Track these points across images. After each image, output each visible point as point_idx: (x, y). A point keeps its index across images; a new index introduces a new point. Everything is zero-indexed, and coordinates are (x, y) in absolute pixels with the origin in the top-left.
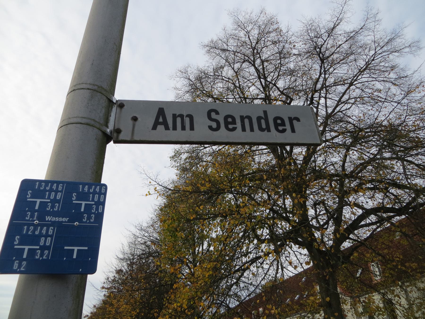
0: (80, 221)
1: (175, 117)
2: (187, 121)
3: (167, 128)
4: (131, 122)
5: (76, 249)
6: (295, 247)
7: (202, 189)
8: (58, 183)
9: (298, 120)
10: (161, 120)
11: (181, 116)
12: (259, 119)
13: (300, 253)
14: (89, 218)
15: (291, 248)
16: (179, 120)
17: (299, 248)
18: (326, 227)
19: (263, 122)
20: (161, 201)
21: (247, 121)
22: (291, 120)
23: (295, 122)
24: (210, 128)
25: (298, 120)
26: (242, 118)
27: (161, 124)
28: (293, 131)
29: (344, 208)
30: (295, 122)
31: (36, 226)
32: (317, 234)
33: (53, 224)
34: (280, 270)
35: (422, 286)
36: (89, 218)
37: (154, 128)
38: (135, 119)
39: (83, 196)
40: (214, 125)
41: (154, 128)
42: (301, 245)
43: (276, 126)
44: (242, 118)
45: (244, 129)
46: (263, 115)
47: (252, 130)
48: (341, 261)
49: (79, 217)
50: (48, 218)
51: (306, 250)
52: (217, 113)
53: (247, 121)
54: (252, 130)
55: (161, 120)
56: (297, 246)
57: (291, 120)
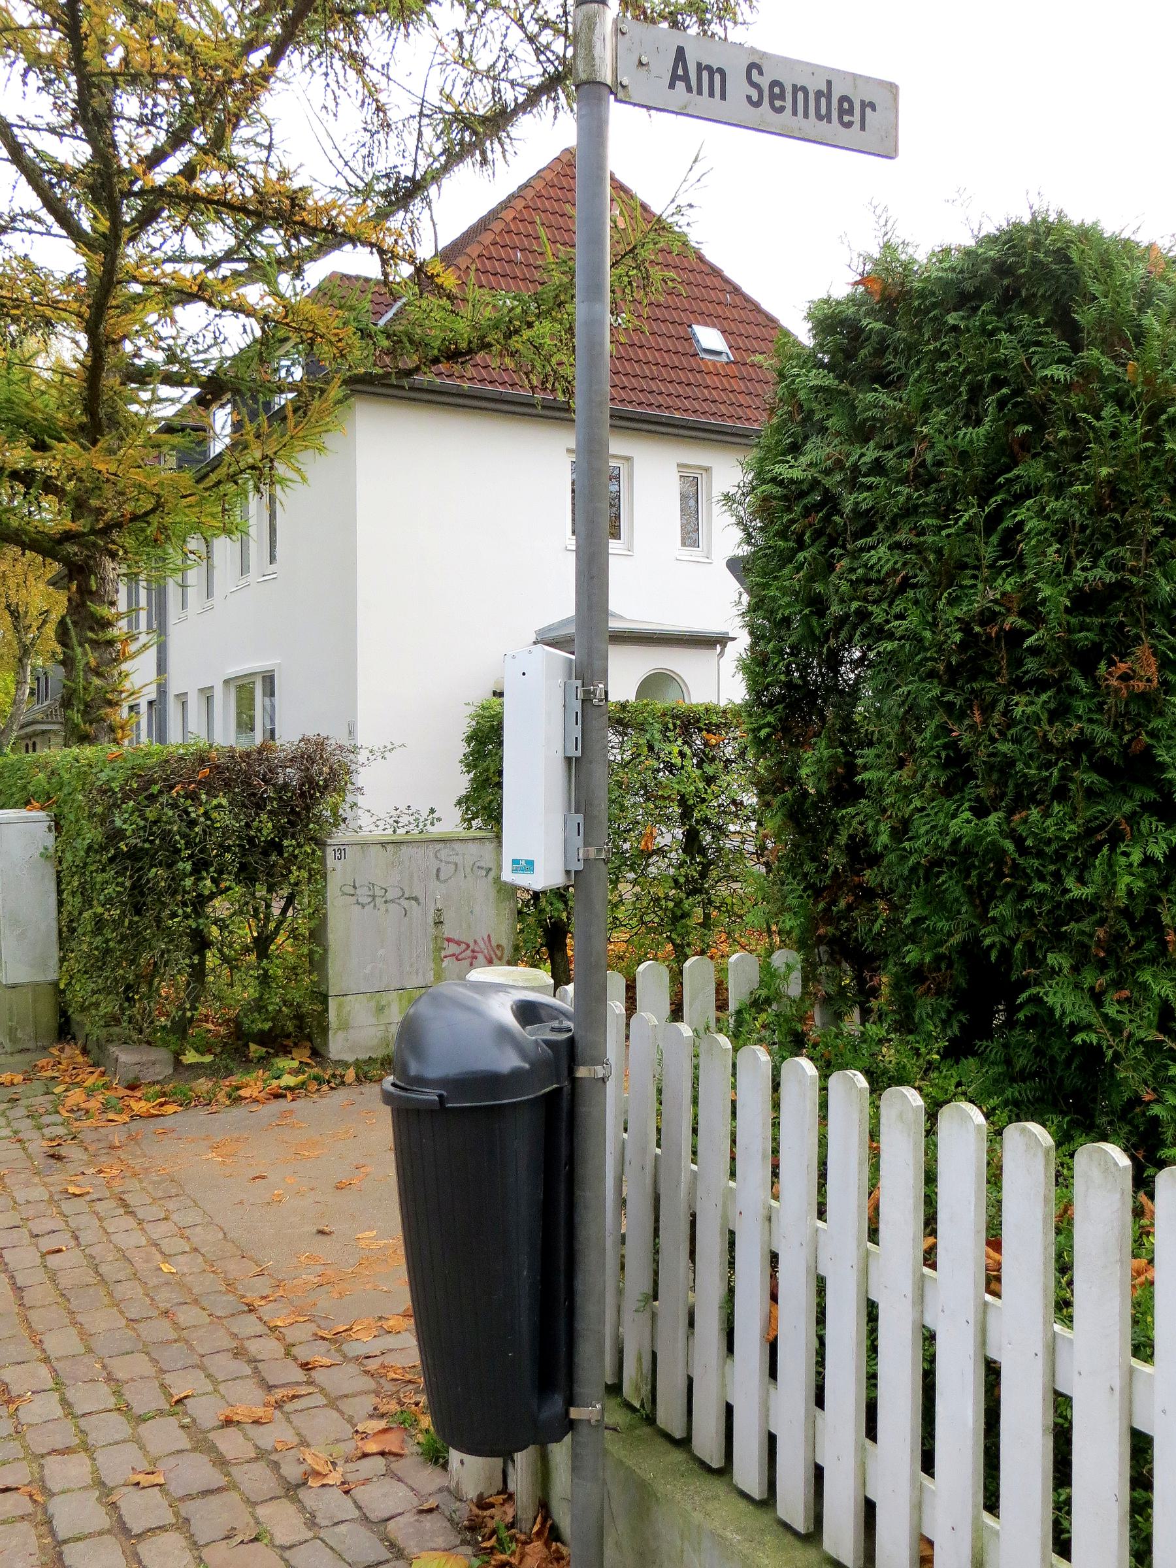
3: (689, 89)
7: (178, 224)
10: (680, 72)
12: (819, 94)
20: (1026, 220)
21: (800, 95)
22: (863, 105)
24: (749, 98)
25: (873, 107)
27: (680, 78)
28: (863, 128)
29: (862, 800)
30: (868, 110)
35: (1162, 988)
43: (842, 112)
44: (795, 89)
45: (795, 113)
46: (825, 89)
47: (806, 115)
52: (761, 73)
53: (800, 95)
54: (806, 115)
55: (680, 72)
57: (863, 105)
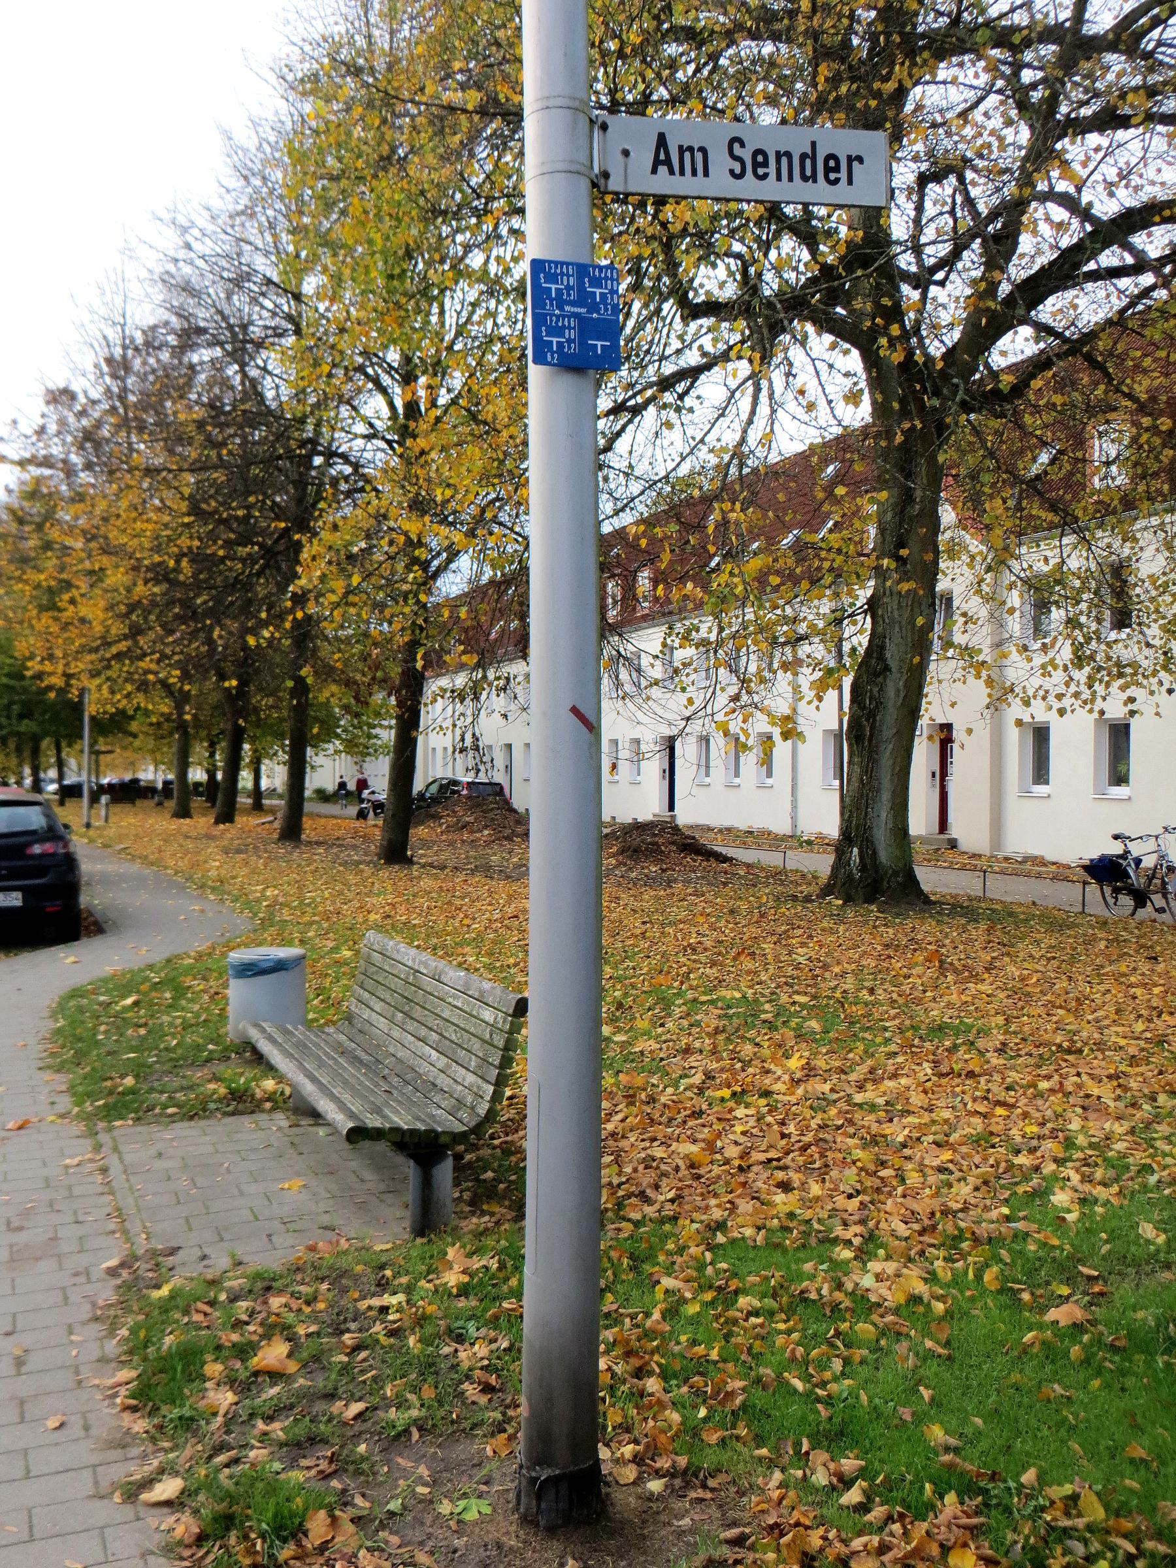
0: (598, 313)
1: (682, 150)
2: (699, 157)
3: (672, 172)
4: (621, 158)
5: (599, 343)
6: (820, 342)
8: (568, 264)
9: (860, 159)
10: (662, 157)
11: (691, 149)
13: (831, 366)
14: (606, 310)
15: (803, 343)
16: (687, 155)
17: (833, 347)
18: (940, 276)
19: (808, 162)
21: (784, 160)
22: (850, 159)
23: (855, 164)
24: (732, 172)
26: (779, 155)
28: (850, 182)
30: (855, 164)
31: (558, 317)
32: (910, 293)
33: (576, 315)
34: (763, 409)
36: (606, 310)
37: (654, 171)
38: (626, 153)
39: (597, 282)
40: (738, 171)
41: (654, 171)
42: (845, 332)
44: (779, 155)
45: (779, 178)
48: (958, 399)
49: (594, 307)
50: (567, 308)
51: (855, 353)
52: (743, 145)
53: (784, 160)
54: (791, 179)
56: (828, 338)
57: (850, 159)
